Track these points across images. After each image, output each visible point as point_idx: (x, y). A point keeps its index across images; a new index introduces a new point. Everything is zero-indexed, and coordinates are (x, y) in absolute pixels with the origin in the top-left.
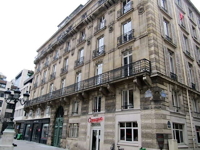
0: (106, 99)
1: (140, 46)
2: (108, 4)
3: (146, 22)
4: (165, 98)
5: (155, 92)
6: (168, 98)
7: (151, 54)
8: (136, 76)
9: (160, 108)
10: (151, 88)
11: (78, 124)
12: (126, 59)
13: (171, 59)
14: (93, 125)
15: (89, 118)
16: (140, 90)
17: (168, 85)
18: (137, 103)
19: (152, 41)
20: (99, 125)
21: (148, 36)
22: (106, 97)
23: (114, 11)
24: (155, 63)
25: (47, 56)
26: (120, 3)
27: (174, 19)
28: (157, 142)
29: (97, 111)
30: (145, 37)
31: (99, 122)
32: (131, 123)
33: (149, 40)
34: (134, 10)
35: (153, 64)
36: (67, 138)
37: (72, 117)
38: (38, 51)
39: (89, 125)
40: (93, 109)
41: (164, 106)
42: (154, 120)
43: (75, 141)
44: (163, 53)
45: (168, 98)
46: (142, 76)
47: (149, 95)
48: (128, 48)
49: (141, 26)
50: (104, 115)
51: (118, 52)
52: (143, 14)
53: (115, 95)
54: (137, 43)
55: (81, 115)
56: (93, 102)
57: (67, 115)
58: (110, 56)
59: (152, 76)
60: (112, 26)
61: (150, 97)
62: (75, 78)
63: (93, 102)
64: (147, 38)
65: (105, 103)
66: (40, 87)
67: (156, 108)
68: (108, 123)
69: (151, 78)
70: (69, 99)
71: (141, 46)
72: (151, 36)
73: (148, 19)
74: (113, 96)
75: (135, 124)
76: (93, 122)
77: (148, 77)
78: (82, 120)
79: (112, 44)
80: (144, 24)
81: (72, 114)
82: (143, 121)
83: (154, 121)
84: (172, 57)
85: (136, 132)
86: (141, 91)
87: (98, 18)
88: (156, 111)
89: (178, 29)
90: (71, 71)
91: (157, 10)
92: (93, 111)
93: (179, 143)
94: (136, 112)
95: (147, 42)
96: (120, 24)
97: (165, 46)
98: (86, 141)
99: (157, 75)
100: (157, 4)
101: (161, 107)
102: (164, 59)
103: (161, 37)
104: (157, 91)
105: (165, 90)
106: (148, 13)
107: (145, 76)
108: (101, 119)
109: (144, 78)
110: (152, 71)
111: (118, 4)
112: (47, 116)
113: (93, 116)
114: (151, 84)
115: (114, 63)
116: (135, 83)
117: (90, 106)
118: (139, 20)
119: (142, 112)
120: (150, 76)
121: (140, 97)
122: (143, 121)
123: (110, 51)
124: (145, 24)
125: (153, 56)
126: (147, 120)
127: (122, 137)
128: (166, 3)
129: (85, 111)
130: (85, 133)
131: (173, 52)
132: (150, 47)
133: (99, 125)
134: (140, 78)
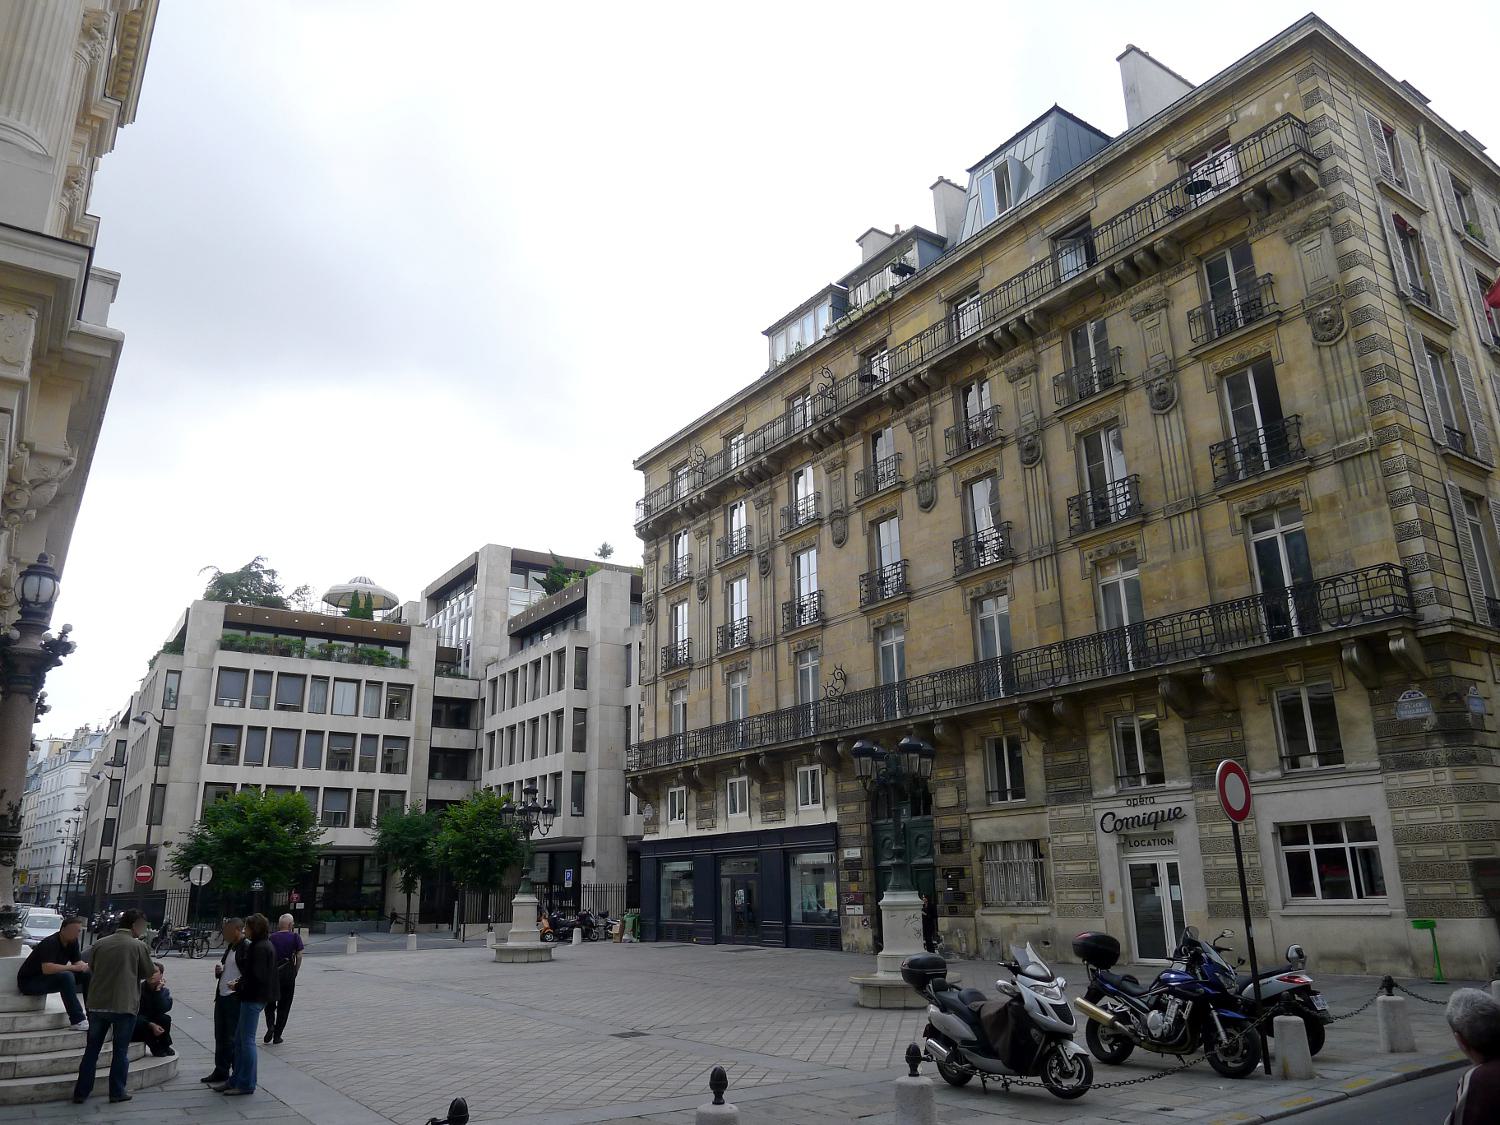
0: (1185, 725)
1: (1345, 498)
2: (1128, 270)
3: (1361, 386)
4: (1486, 717)
5: (1447, 697)
6: (1491, 715)
7: (1404, 533)
8: (1352, 635)
9: (1474, 762)
10: (1423, 681)
11: (1035, 843)
12: (1267, 551)
13: (1475, 529)
14: (1127, 843)
15: (1105, 812)
16: (1370, 689)
17: (1485, 657)
18: (1361, 740)
19: (1405, 480)
20: (1168, 840)
21: (1382, 453)
22: (1184, 718)
23: (1166, 306)
24: (1432, 576)
25: (730, 499)
26: (1194, 269)
27: (1462, 329)
28: (1476, 893)
29: (1144, 782)
30: (1366, 459)
31: (1165, 828)
32: (1305, 826)
33: (1387, 474)
34: (1284, 318)
35: (1424, 581)
36: (978, 912)
37: (989, 811)
38: (645, 464)
39: (1108, 844)
40: (1115, 772)
41: (1484, 751)
42: (1450, 808)
43: (1034, 919)
44: (1447, 518)
45: (1491, 715)
46: (1384, 638)
47: (1414, 707)
48: (1279, 501)
49: (1336, 405)
50: (1189, 797)
51: (1221, 517)
52: (1342, 347)
53: (1237, 711)
54: (1323, 482)
55: (1047, 799)
56: (1111, 739)
57: (958, 806)
58: (1176, 531)
59: (1423, 633)
60: (1167, 385)
61: (1424, 720)
62: (974, 628)
63: (1111, 739)
64: (1377, 462)
65: (1183, 742)
66: (718, 669)
67: (1453, 761)
68: (1215, 829)
69: (1420, 640)
70: (947, 736)
71: (1349, 499)
72: (1393, 454)
73: (1370, 376)
74: (1229, 715)
75: (1362, 828)
76: (1131, 832)
77: (1410, 637)
78: (1061, 827)
79: (1181, 472)
80: (1353, 399)
81: (988, 800)
82: (1399, 817)
83: (1455, 814)
84: (1476, 520)
85: (1369, 857)
86: (1377, 692)
87: (1064, 330)
88: (1458, 775)
89: (1484, 373)
90: (937, 588)
91: (1397, 314)
92: (1117, 784)
93: (1311, 892)
94: (1360, 780)
95: (1380, 481)
96: (1213, 378)
97: (1451, 483)
98: (1101, 915)
99: (1448, 629)
100: (1390, 287)
101: (1475, 757)
102: (1458, 548)
103: (1431, 448)
104: (1455, 694)
105: (1477, 683)
106: (1367, 345)
107: (1398, 638)
108: (1176, 816)
109: (1393, 646)
110: (1421, 611)
111: (1181, 271)
112: (813, 815)
113: (1124, 803)
114: (1423, 667)
115: (1208, 568)
116: (1352, 665)
117: (1095, 761)
118: (1324, 375)
119: (1391, 781)
120: (1414, 631)
121: (1374, 717)
122: (1399, 817)
123: (1178, 507)
124: (1354, 399)
125: (1417, 546)
126: (1420, 810)
127: (1300, 884)
128: (1418, 253)
129: (1070, 784)
130: (1094, 882)
131: (1480, 499)
132: (1396, 502)
133: (1168, 840)
134: (1373, 646)
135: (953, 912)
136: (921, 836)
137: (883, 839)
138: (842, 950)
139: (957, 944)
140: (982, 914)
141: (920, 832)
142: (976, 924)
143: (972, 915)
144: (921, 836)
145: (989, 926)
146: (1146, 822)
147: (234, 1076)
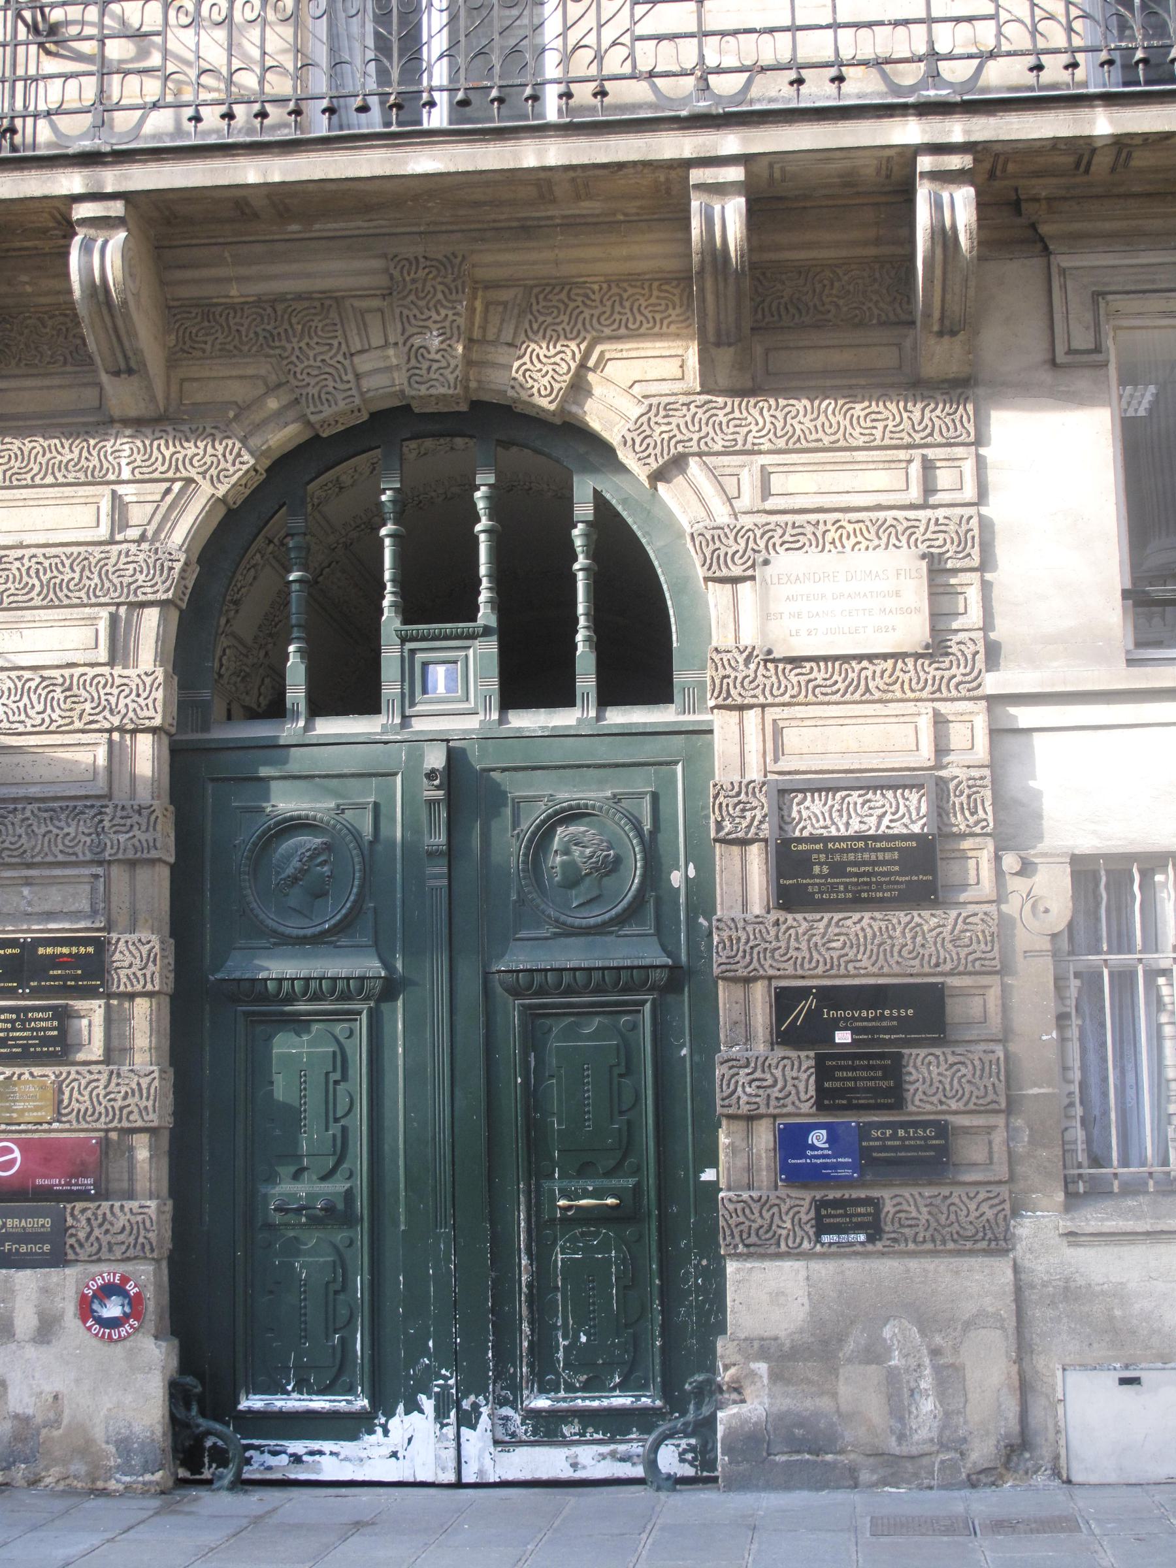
135: (843, 1220)
136: (571, 815)
137: (530, 821)
138: (1111, 1193)
139: (874, 1408)
140: (1072, 1237)
141: (567, 795)
142: (1018, 1290)
143: (994, 1240)
144: (571, 815)
145: (1119, 1294)
146: (998, 173)
147: (614, 1196)
